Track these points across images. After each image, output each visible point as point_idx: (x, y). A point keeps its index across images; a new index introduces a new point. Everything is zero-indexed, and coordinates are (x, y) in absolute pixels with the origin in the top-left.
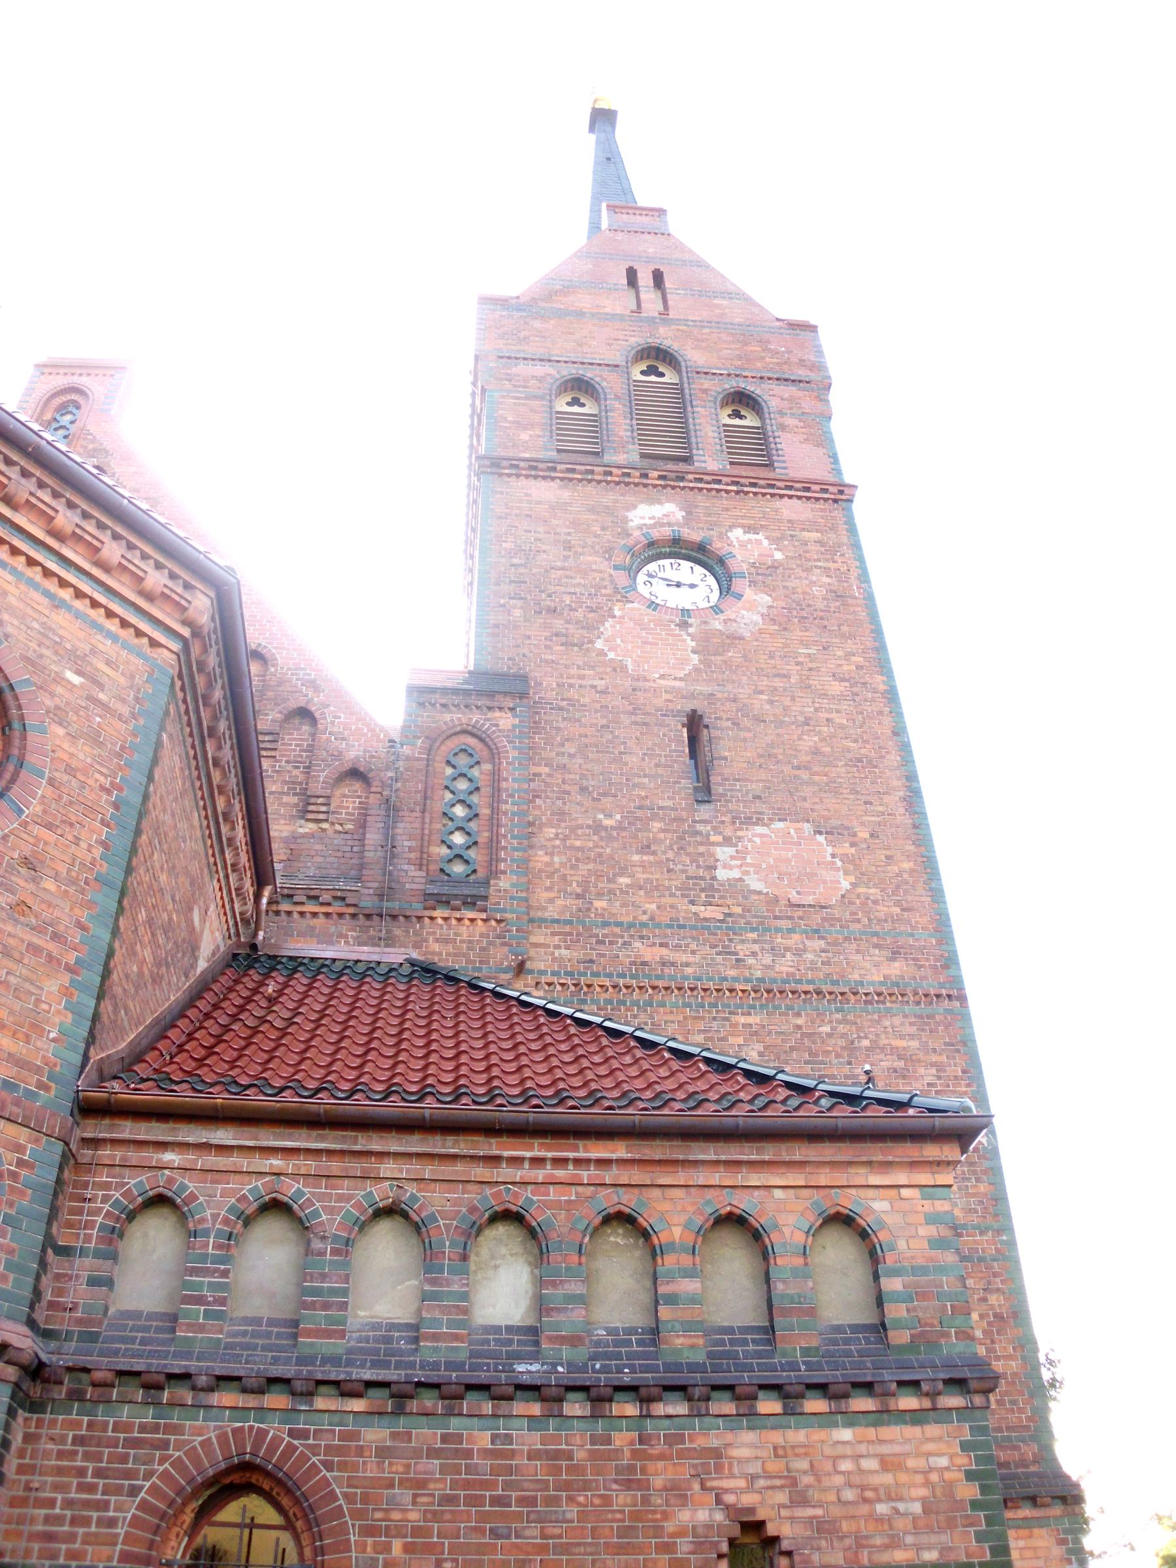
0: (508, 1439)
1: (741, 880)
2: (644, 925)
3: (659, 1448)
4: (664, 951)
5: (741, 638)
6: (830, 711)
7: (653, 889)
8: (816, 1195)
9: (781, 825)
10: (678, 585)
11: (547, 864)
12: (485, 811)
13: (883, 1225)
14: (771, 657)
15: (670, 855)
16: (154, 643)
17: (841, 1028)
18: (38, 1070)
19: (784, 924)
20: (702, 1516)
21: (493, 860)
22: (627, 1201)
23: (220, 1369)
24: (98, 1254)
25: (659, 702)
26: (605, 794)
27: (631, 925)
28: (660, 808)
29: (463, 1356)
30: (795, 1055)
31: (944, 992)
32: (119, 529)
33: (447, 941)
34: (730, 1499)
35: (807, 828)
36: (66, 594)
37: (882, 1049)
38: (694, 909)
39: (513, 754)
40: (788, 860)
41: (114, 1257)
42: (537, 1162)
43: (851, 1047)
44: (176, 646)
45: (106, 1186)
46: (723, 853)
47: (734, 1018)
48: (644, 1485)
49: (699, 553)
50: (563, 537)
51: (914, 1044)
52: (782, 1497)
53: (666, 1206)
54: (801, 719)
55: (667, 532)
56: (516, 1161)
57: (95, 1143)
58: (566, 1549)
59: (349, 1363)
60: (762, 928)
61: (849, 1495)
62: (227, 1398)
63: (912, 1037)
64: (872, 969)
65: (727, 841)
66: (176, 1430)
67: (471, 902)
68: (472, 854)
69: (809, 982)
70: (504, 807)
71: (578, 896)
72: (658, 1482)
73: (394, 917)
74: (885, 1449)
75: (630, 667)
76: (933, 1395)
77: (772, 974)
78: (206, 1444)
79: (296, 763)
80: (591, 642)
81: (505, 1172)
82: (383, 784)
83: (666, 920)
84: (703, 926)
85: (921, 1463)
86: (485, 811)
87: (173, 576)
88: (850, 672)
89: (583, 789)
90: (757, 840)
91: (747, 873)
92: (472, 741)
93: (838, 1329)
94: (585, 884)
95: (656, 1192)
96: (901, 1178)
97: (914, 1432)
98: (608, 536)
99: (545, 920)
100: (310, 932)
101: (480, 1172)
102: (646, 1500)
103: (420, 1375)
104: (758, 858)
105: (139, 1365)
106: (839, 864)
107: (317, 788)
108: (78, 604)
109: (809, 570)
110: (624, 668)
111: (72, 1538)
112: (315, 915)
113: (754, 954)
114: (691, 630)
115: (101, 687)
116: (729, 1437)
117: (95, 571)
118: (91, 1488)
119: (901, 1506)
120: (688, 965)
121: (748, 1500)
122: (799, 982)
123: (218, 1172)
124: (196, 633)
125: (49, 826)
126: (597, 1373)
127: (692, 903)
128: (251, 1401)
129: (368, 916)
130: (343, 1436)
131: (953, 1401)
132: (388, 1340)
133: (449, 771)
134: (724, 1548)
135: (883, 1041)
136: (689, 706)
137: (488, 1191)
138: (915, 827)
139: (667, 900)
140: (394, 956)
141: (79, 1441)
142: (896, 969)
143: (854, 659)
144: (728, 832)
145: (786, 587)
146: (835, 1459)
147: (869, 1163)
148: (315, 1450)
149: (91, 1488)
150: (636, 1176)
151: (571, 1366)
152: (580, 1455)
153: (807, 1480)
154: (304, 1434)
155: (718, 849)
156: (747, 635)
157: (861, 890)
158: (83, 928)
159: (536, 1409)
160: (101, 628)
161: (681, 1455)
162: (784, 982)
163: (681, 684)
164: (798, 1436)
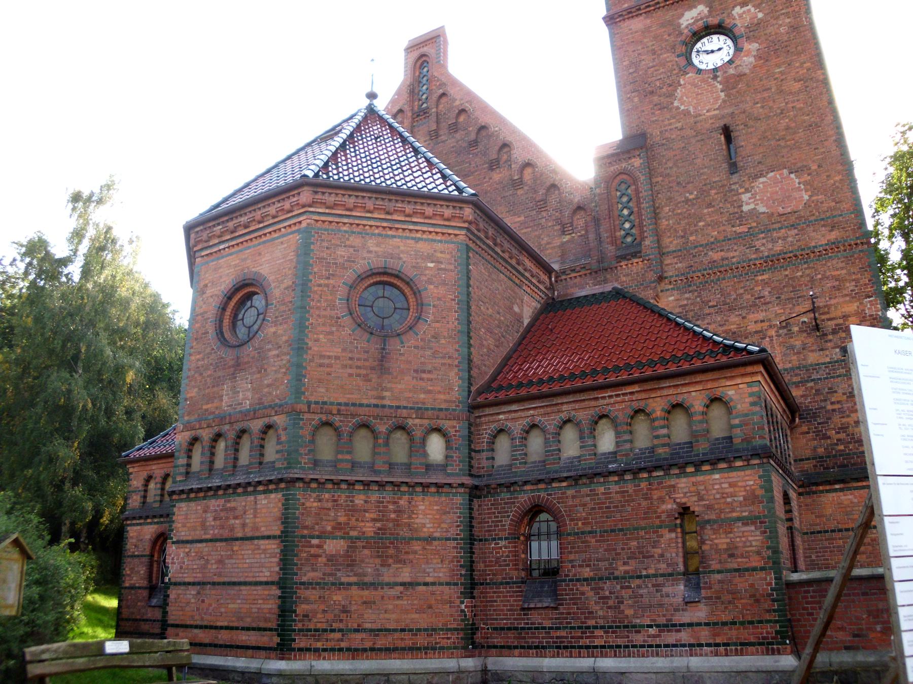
0: (609, 489)
1: (755, 209)
2: (712, 243)
3: (655, 486)
4: (723, 253)
5: (745, 74)
6: (793, 102)
7: (715, 224)
8: (707, 392)
9: (772, 174)
10: (712, 52)
11: (668, 225)
12: (636, 209)
13: (732, 400)
14: (761, 80)
15: (721, 205)
16: (456, 235)
17: (807, 272)
18: (455, 402)
19: (776, 226)
20: (669, 506)
21: (642, 232)
22: (641, 405)
23: (524, 479)
24: (488, 450)
25: (708, 126)
26: (688, 183)
27: (707, 245)
28: (714, 182)
29: (594, 465)
30: (785, 289)
31: (859, 242)
32: (429, 202)
33: (628, 275)
34: (678, 500)
35: (785, 172)
36: (419, 235)
37: (827, 278)
38: (734, 229)
39: (642, 178)
40: (777, 192)
41: (493, 450)
42: (610, 397)
43: (812, 280)
44: (463, 232)
45: (486, 429)
46: (745, 197)
47: (756, 278)
48: (651, 499)
49: (719, 29)
50: (650, 48)
51: (844, 271)
52: (695, 499)
53: (655, 404)
54: (779, 111)
55: (700, 24)
56: (604, 398)
57: (480, 417)
58: (628, 520)
59: (561, 472)
60: (767, 231)
61: (718, 496)
62: (527, 487)
63: (842, 268)
64: (821, 237)
65: (747, 191)
66: (517, 498)
67: (635, 255)
68: (633, 231)
69: (791, 252)
70: (642, 206)
71: (682, 237)
72: (655, 497)
73: (606, 270)
74: (731, 480)
75: (692, 111)
76: (748, 460)
77: (772, 252)
78: (525, 501)
79: (556, 210)
80: (672, 103)
81: (601, 402)
82: (592, 211)
83: (722, 238)
84: (739, 236)
85: (744, 484)
86: (636, 209)
87: (454, 207)
88: (803, 74)
89: (679, 183)
90: (761, 186)
91: (757, 204)
92: (624, 176)
93: (717, 439)
94: (684, 231)
95: (651, 400)
96: (739, 381)
97: (742, 473)
98: (672, 39)
99: (668, 252)
100: (575, 285)
101: (593, 403)
102: (652, 503)
103: (580, 473)
104: (763, 195)
105: (503, 481)
106: (803, 187)
107: (566, 220)
108: (425, 236)
109: (777, 18)
110: (689, 112)
111: (495, 530)
112: (575, 277)
113: (763, 245)
114: (719, 79)
115: (441, 263)
116: (677, 480)
117: (426, 221)
118: (497, 517)
119: (736, 499)
120: (733, 257)
121: (684, 500)
122: (786, 253)
123: (515, 418)
124: (470, 223)
125: (437, 322)
126: (634, 465)
127: (733, 226)
128: (535, 487)
129: (596, 272)
130: (562, 494)
131: (756, 461)
132: (572, 462)
133: (618, 194)
134: (677, 516)
135: (828, 274)
136: (722, 124)
137: (597, 409)
138: (842, 155)
139: (722, 228)
140: (608, 288)
141: (492, 505)
142: (833, 235)
143: (805, 65)
144: (747, 186)
145: (766, 34)
146: (713, 485)
147: (725, 378)
148: (554, 498)
149: (497, 517)
150: (644, 396)
151: (626, 464)
152: (631, 491)
153: (703, 492)
154: (551, 495)
155: (743, 196)
156: (747, 71)
157: (814, 198)
158: (458, 351)
159: (616, 478)
160: (435, 241)
161: (662, 488)
162: (779, 255)
163: (716, 112)
164: (700, 478)
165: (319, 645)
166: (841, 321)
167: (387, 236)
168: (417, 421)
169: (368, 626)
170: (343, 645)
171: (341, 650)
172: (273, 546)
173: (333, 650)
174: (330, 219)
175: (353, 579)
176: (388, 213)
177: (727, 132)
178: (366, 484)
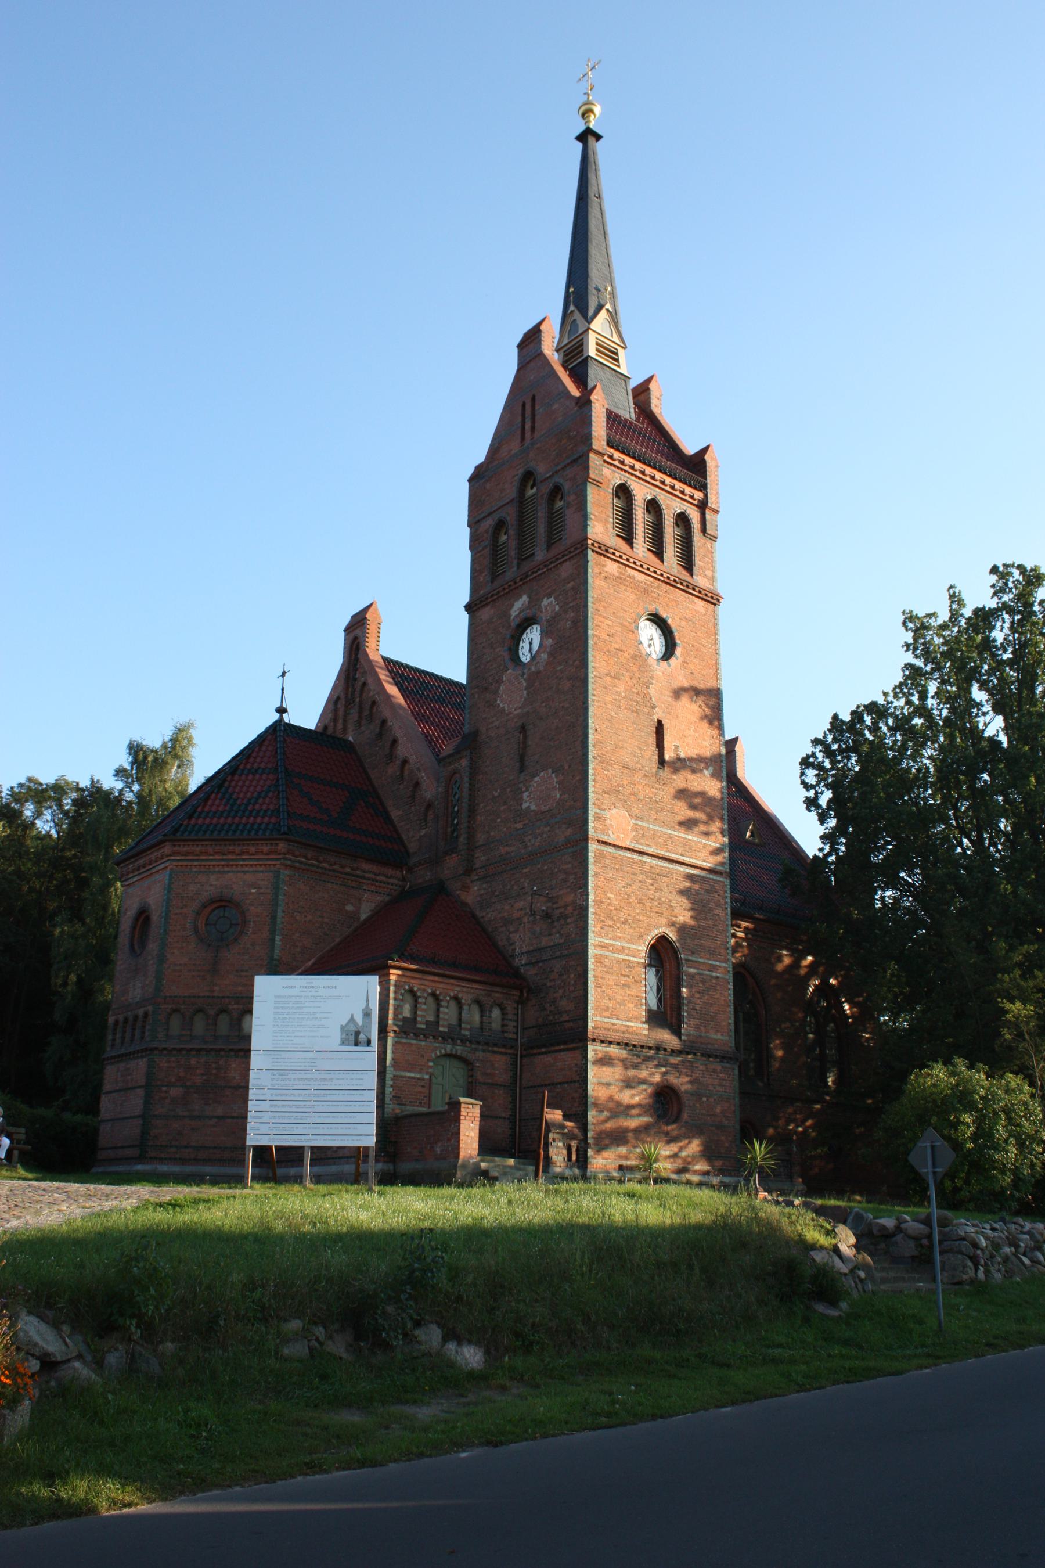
51: (570, 866)
165: (163, 1155)
166: (562, 910)
167: (224, 872)
168: (235, 1006)
169: (194, 1144)
170: (178, 1156)
171: (175, 1159)
172: (141, 1092)
173: (170, 1159)
174: (185, 863)
175: (186, 1114)
176: (224, 854)
177: (523, 729)
178: (199, 1050)
